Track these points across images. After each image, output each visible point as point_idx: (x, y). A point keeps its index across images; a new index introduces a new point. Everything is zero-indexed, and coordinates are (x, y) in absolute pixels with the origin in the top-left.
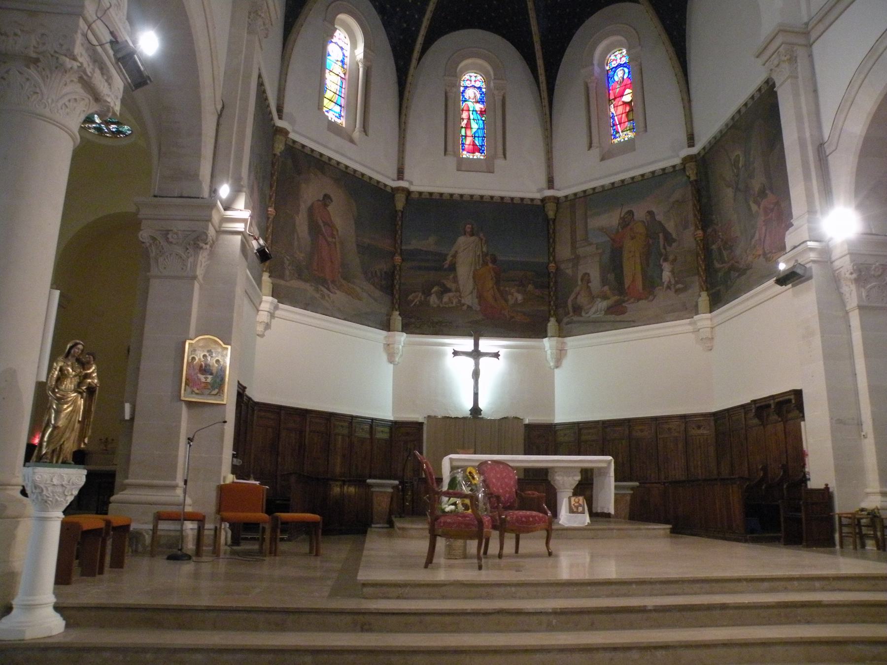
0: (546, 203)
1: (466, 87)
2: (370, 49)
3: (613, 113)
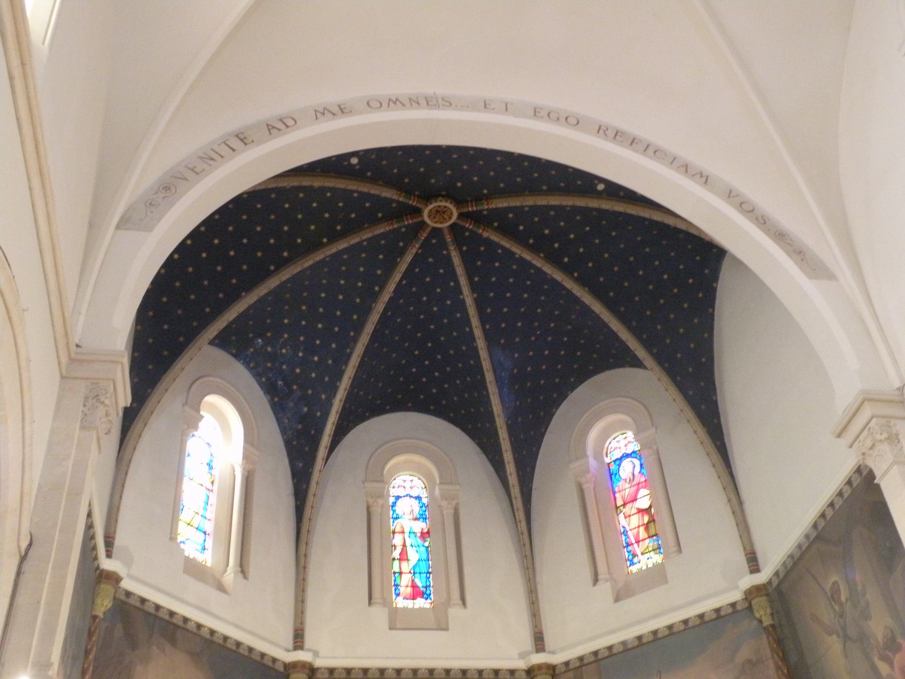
0: (536, 676)
1: (398, 498)
2: (252, 445)
3: (624, 527)
